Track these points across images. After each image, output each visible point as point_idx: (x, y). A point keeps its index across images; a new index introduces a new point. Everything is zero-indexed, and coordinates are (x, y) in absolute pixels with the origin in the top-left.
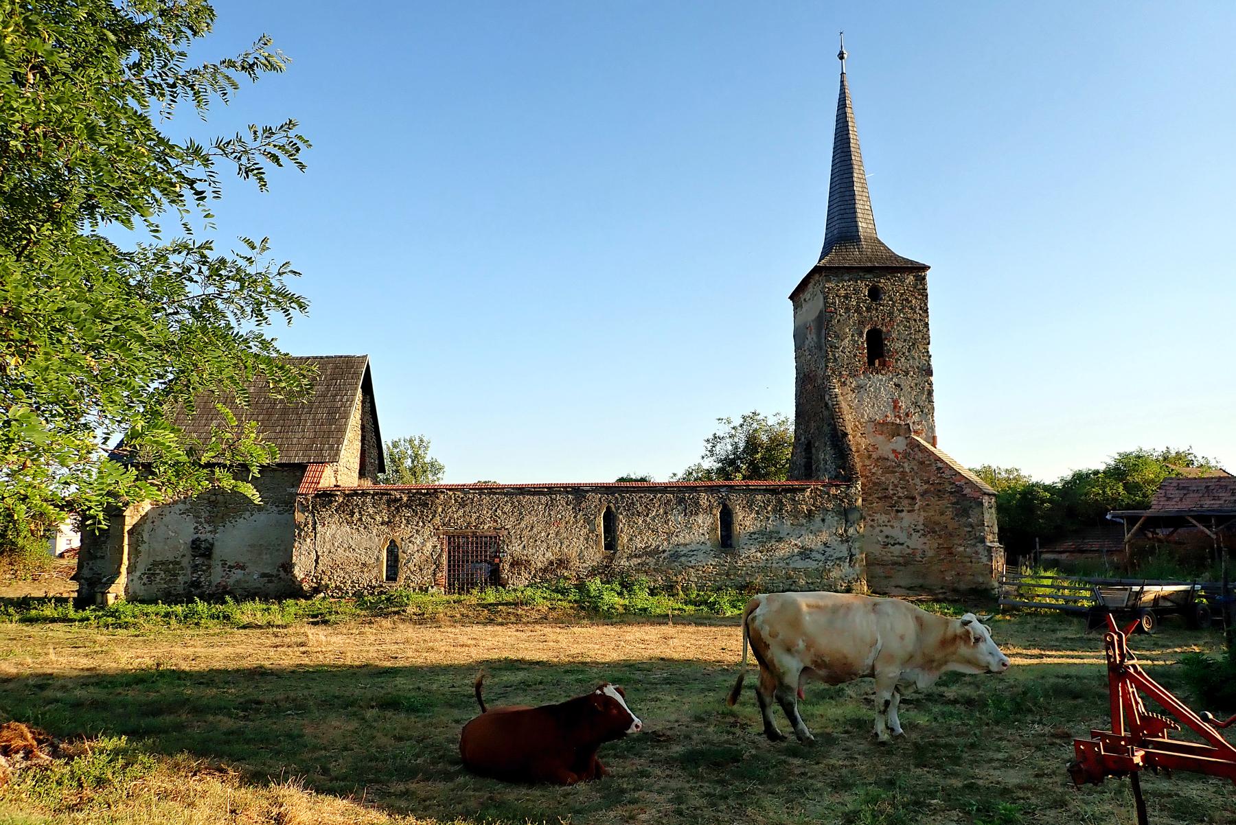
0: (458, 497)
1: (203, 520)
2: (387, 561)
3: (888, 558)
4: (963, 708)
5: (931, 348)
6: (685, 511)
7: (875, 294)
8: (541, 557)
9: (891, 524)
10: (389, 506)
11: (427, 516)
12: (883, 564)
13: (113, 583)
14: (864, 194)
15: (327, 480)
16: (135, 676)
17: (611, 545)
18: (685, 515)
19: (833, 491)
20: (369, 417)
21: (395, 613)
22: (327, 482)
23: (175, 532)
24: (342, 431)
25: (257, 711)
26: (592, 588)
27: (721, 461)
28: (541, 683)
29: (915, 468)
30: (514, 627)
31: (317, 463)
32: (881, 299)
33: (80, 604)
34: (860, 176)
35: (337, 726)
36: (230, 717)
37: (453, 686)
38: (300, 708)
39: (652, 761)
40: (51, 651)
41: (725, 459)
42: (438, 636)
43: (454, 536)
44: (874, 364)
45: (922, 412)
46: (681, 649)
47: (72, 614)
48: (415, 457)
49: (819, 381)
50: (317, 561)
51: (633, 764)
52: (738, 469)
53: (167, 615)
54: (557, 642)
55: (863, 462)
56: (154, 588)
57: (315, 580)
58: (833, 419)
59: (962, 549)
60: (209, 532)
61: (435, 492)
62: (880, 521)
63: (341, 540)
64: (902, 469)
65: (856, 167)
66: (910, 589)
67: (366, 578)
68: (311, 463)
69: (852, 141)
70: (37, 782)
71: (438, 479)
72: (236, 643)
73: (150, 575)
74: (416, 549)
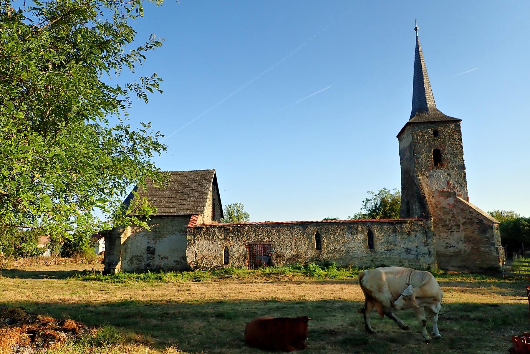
0: (253, 228)
1: (151, 239)
2: (224, 255)
3: (448, 253)
4: (478, 323)
5: (464, 157)
6: (352, 233)
7: (436, 133)
8: (289, 253)
9: (449, 237)
10: (224, 232)
11: (240, 236)
12: (445, 256)
13: (117, 264)
14: (429, 89)
15: (199, 221)
16: (122, 302)
17: (319, 247)
18: (352, 234)
19: (420, 223)
20: (216, 195)
21: (228, 277)
22: (199, 222)
23: (140, 244)
24: (205, 201)
25: (167, 317)
26: (311, 267)
27: (369, 210)
28: (285, 308)
29: (459, 212)
30: (277, 284)
31: (195, 214)
32: (439, 136)
33: (105, 273)
34: (427, 81)
35: (198, 324)
36: (155, 319)
37: (248, 309)
38: (184, 316)
39: (328, 343)
40: (92, 292)
41: (372, 209)
42: (244, 287)
43: (252, 245)
44: (437, 165)
45: (461, 186)
46: (349, 294)
47: (102, 277)
48: (238, 212)
49: (412, 174)
50: (196, 256)
51: (319, 344)
52: (378, 214)
53: (137, 278)
54: (295, 290)
55: (434, 209)
56: (133, 266)
57: (195, 264)
58: (419, 190)
59: (483, 249)
60: (153, 244)
61: (243, 226)
62: (444, 236)
63: (205, 246)
64: (452, 212)
65: (425, 77)
66: (459, 267)
67: (216, 262)
68: (193, 215)
69: (422, 66)
70: (75, 343)
71: (248, 220)
72: (162, 289)
73: (131, 261)
74: (236, 250)
